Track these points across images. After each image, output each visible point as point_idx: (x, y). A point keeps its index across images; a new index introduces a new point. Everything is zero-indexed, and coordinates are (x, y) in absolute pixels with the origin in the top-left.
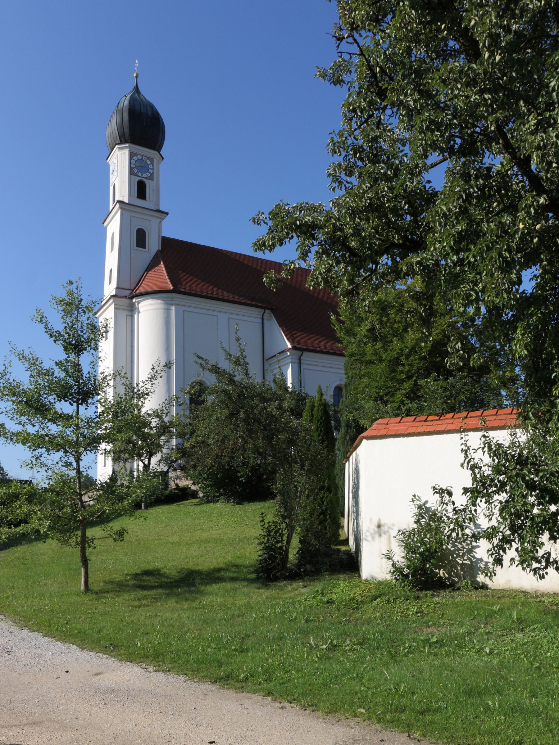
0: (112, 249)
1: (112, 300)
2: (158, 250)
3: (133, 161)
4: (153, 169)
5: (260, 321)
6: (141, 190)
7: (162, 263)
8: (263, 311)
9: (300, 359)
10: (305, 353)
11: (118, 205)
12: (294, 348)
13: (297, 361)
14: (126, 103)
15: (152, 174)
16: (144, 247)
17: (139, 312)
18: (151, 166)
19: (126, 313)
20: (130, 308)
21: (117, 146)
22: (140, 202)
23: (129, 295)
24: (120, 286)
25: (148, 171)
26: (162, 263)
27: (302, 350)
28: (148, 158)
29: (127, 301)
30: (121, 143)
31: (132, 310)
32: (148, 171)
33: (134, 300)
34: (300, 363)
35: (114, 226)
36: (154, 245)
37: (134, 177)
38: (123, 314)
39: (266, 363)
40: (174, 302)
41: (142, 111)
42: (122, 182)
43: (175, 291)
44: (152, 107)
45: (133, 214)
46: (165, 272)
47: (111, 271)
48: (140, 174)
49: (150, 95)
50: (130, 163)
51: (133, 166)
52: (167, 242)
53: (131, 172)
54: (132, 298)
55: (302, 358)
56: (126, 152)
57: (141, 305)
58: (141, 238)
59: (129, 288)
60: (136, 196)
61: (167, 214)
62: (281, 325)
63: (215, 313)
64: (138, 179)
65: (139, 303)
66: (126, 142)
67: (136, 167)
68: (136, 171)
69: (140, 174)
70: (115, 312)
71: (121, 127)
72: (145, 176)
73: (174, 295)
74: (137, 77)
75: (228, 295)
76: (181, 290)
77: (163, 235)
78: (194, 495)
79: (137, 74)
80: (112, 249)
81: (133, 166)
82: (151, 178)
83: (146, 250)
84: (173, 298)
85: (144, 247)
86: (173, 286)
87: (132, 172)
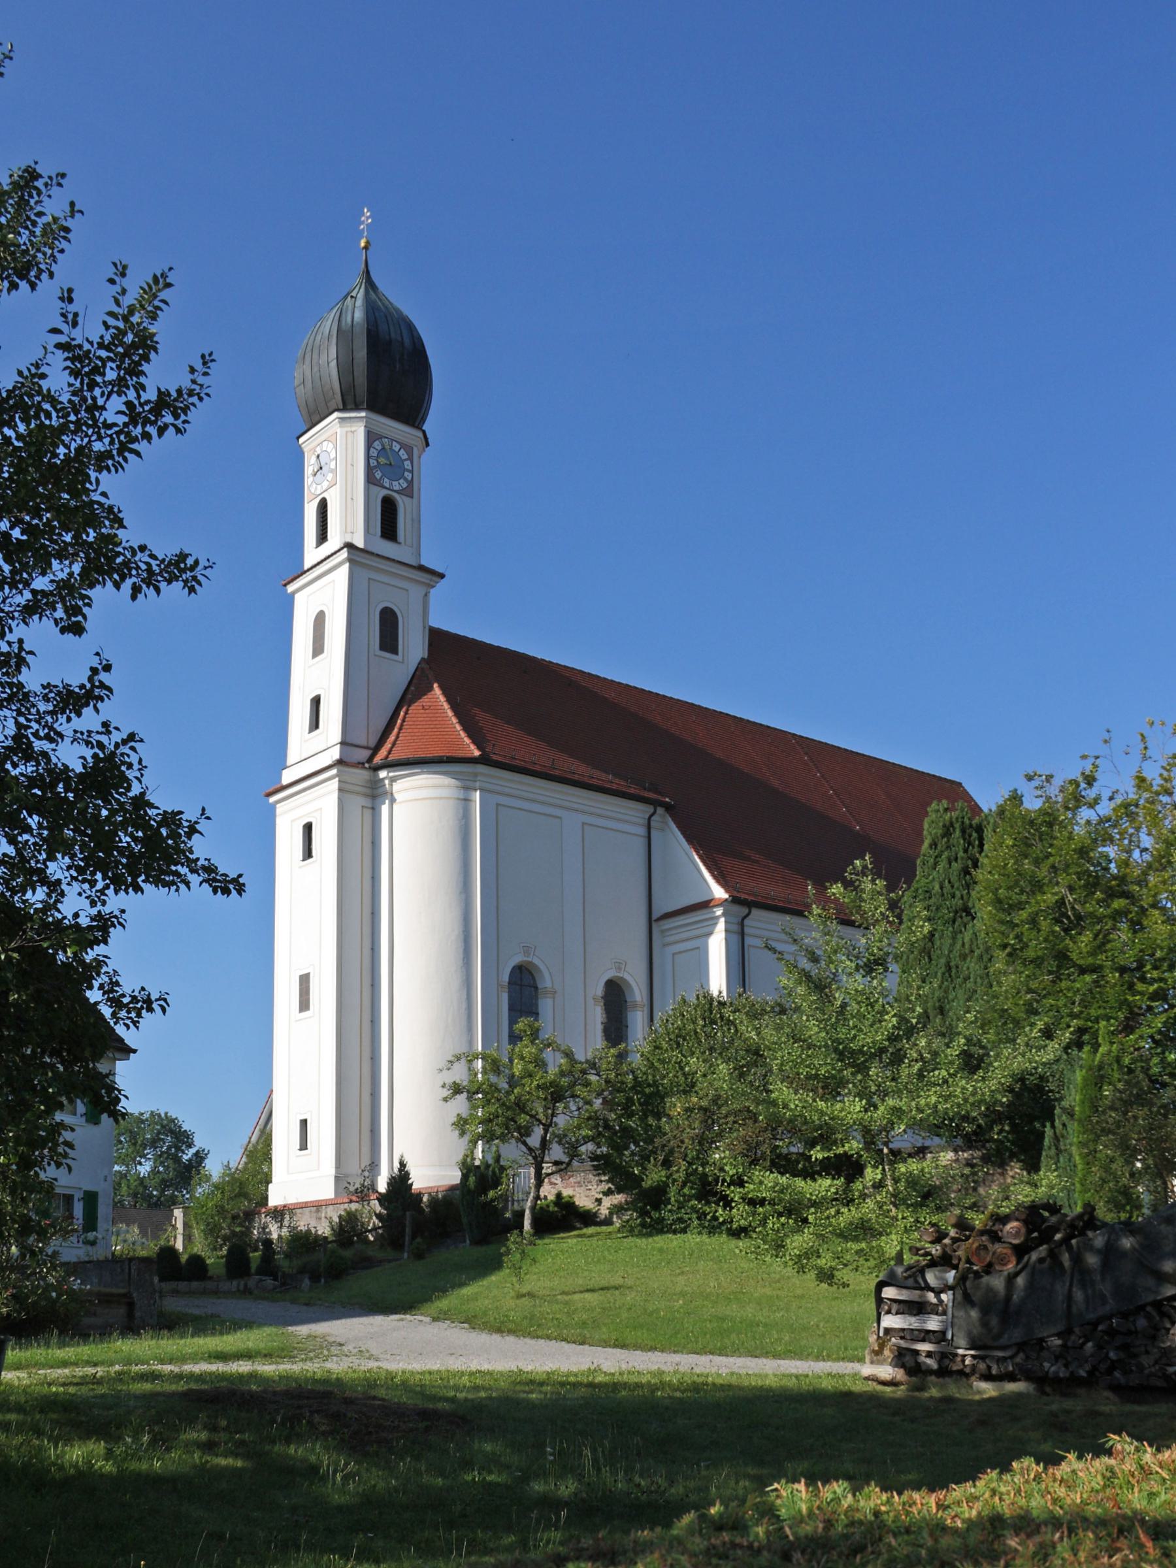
0: (318, 648)
1: (334, 771)
2: (423, 659)
3: (374, 453)
4: (412, 471)
5: (642, 831)
6: (387, 519)
7: (435, 685)
8: (651, 809)
9: (742, 924)
10: (756, 912)
11: (344, 554)
12: (735, 900)
13: (736, 928)
14: (359, 315)
15: (410, 483)
16: (394, 651)
17: (393, 801)
18: (407, 465)
19: (367, 802)
20: (368, 791)
21: (336, 415)
22: (386, 548)
23: (368, 761)
24: (348, 740)
25: (402, 476)
26: (435, 685)
27: (750, 905)
28: (403, 446)
29: (362, 775)
30: (344, 409)
31: (376, 794)
32: (402, 476)
33: (383, 774)
34: (742, 934)
35: (324, 597)
36: (414, 648)
37: (375, 489)
38: (358, 802)
39: (654, 925)
40: (478, 784)
41: (393, 335)
42: (347, 499)
43: (484, 760)
44: (411, 327)
45: (374, 575)
46: (450, 713)
47: (316, 701)
48: (387, 483)
49: (401, 298)
50: (368, 457)
51: (373, 463)
52: (438, 639)
53: (370, 479)
54: (377, 769)
55: (746, 922)
56: (359, 432)
57: (397, 786)
58: (389, 629)
59: (364, 743)
60: (379, 533)
61: (442, 576)
62: (689, 840)
63: (558, 812)
64: (384, 492)
65: (393, 780)
66: (357, 408)
67: (382, 467)
68: (378, 475)
69: (387, 483)
70: (339, 799)
71: (346, 368)
72: (396, 488)
73: (481, 768)
74: (366, 248)
75: (581, 770)
76: (495, 757)
77: (436, 622)
78: (588, 1218)
79: (368, 243)
80: (318, 648)
81: (373, 463)
82: (408, 492)
83: (399, 658)
84: (476, 775)
85: (394, 651)
86: (479, 748)
87: (370, 479)
